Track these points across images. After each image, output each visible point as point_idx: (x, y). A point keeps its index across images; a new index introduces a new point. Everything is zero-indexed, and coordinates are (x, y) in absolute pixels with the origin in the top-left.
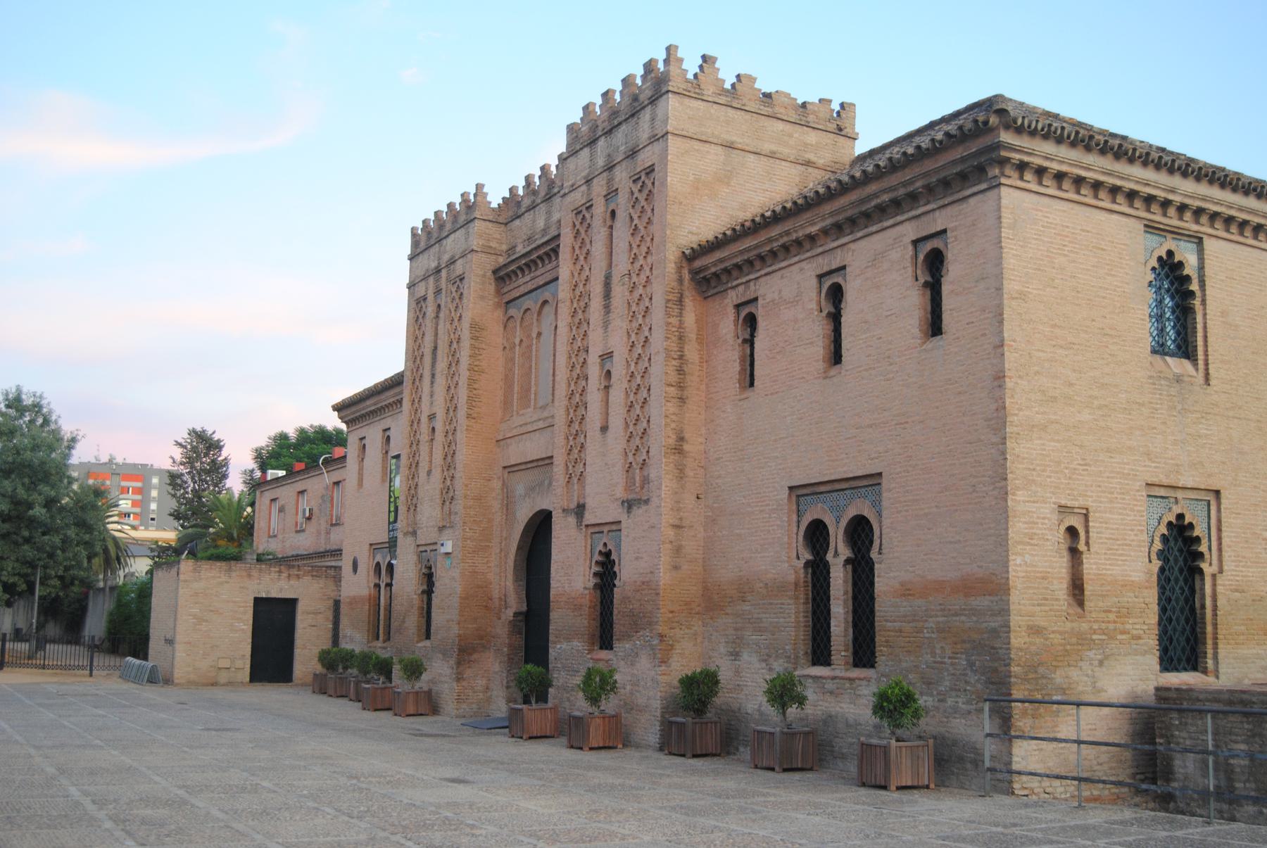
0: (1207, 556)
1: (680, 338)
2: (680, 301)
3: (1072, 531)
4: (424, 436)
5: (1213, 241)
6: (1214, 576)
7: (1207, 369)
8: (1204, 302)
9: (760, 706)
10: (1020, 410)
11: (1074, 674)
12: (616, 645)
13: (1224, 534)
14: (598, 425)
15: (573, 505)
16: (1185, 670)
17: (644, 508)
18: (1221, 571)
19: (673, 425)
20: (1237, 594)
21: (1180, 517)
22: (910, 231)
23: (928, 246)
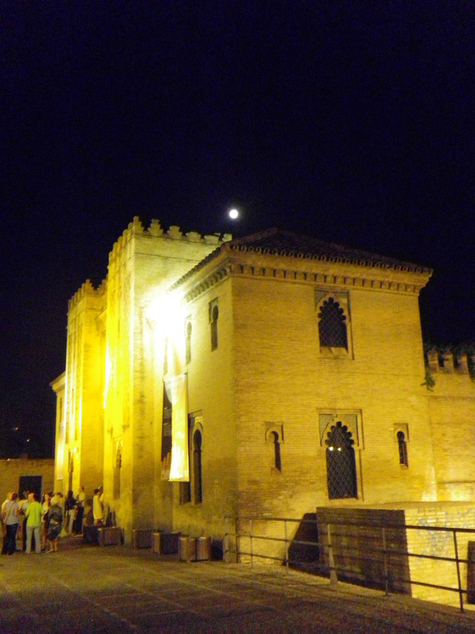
0: (356, 441)
1: (141, 350)
2: (141, 332)
3: (276, 434)
5: (355, 291)
6: (360, 451)
7: (353, 352)
8: (350, 320)
10: (242, 379)
11: (275, 502)
13: (364, 430)
16: (347, 497)
18: (364, 449)
19: (138, 390)
20: (374, 459)
21: (339, 424)
22: (95, 313)
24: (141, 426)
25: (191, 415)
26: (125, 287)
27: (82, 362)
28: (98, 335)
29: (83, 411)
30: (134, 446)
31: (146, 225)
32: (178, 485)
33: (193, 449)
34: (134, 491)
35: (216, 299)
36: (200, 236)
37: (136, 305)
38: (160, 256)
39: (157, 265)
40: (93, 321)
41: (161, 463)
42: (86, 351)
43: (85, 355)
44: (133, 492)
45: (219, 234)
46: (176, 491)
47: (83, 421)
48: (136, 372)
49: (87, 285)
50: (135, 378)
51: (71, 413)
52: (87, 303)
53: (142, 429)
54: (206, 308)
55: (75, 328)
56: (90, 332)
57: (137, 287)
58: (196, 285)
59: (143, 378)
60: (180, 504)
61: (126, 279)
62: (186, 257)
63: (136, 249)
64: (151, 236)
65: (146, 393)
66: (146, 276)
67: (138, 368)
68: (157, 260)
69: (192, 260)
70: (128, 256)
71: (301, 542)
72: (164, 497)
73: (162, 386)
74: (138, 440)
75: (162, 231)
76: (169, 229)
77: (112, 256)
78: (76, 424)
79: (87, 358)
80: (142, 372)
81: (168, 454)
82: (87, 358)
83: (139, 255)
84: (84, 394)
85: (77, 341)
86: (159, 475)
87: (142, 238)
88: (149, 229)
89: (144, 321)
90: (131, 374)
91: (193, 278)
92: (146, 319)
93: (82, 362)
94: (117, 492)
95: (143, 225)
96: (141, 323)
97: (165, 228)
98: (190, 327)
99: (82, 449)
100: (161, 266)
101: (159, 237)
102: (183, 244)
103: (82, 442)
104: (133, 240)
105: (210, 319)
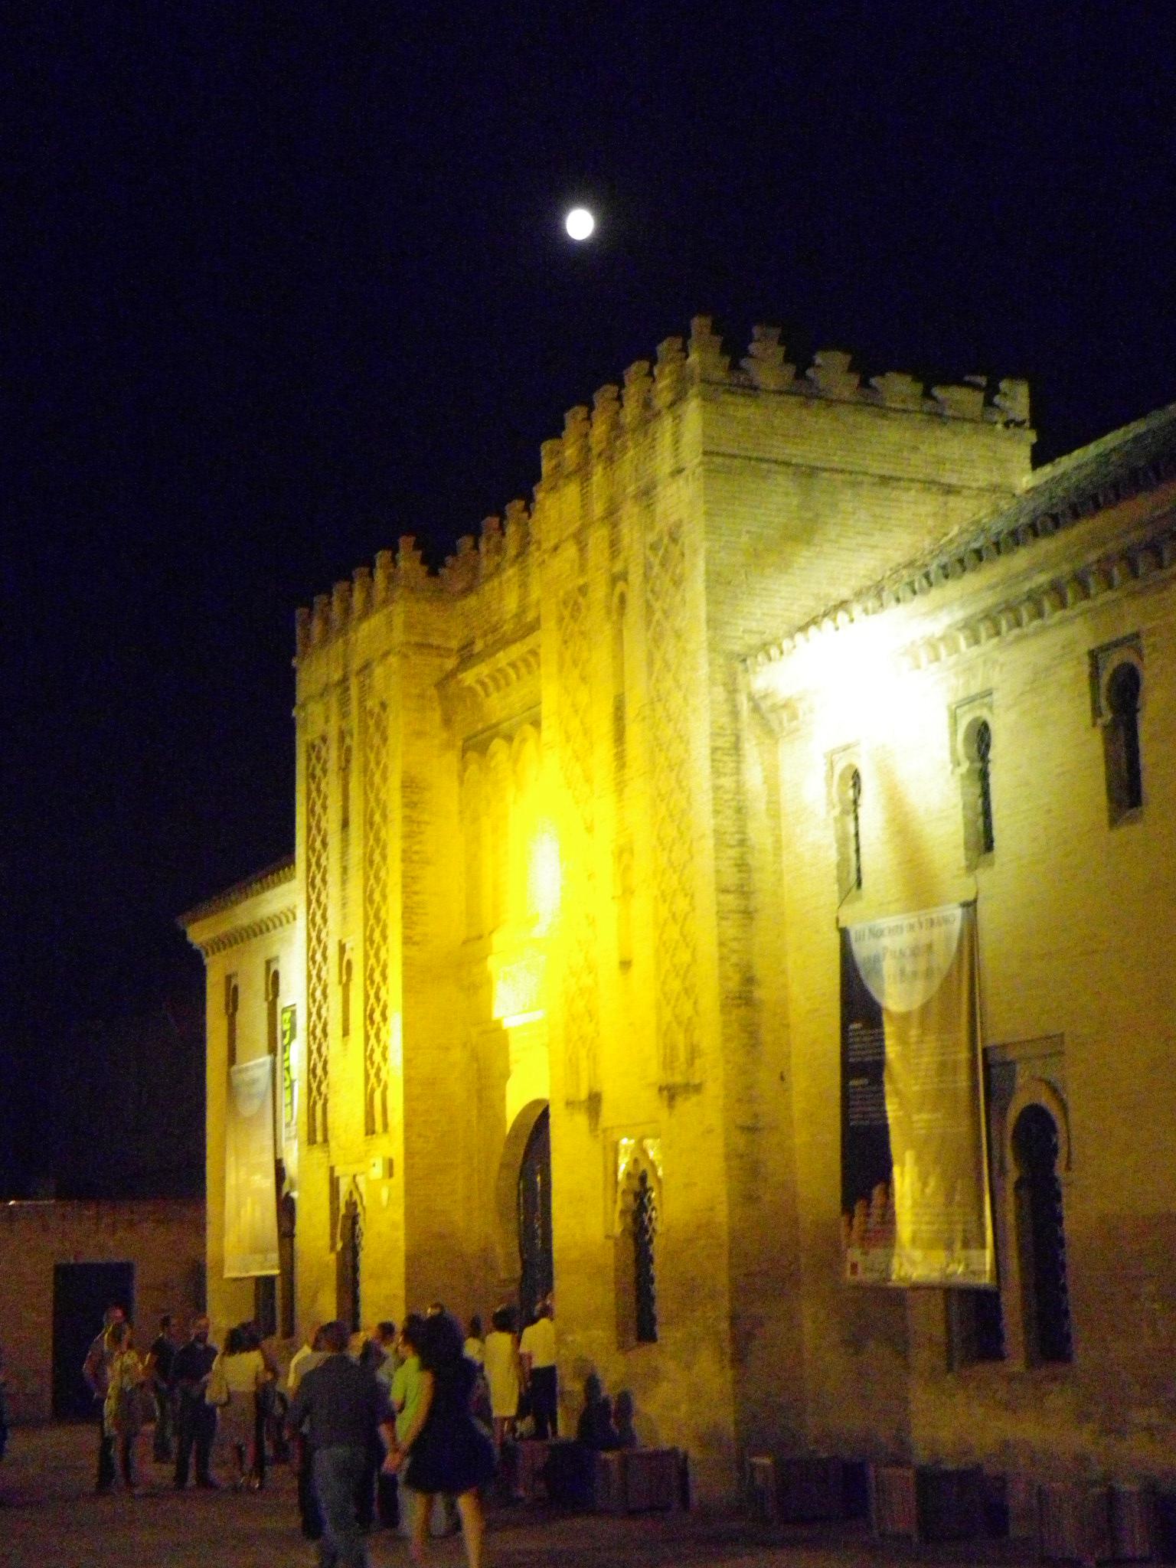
1: (739, 810)
2: (736, 747)
4: (331, 972)
9: (990, 708)
12: (661, 1332)
14: (636, 970)
15: (583, 1095)
17: (694, 1099)
19: (734, 959)
22: (437, 661)
23: (1115, 659)
24: (750, 1087)
25: (990, 1054)
26: (646, 577)
27: (395, 848)
28: (448, 746)
29: (407, 1026)
30: (727, 1157)
31: (735, 349)
32: (939, 1299)
33: (1013, 1174)
34: (734, 1319)
35: (1132, 640)
36: (918, 388)
37: (713, 648)
38: (787, 464)
39: (779, 498)
40: (432, 692)
41: (844, 1220)
42: (410, 805)
43: (408, 820)
44: (732, 1325)
45: (982, 380)
46: (929, 1324)
47: (408, 1062)
48: (724, 891)
49: (408, 560)
50: (722, 916)
51: (335, 1029)
52: (409, 627)
53: (751, 1100)
54: (1074, 673)
55: (345, 715)
56: (420, 734)
57: (716, 580)
58: (1027, 586)
59: (748, 915)
60: (950, 1368)
61: (654, 547)
62: (877, 468)
63: (707, 437)
64: (756, 389)
65: (759, 972)
66: (745, 538)
67: (731, 878)
68: (780, 479)
69: (899, 479)
70: (664, 464)
71: (376, 1485)
72: (855, 1343)
73: (835, 939)
74: (741, 1141)
75: (791, 369)
76: (810, 364)
77: (558, 455)
78: (372, 1075)
79: (413, 830)
80: (744, 891)
81: (877, 1192)
82: (413, 830)
83: (719, 460)
84: (407, 963)
85: (355, 766)
86: (832, 1258)
87: (728, 398)
88: (744, 363)
89: (745, 706)
90: (707, 899)
91: (1020, 559)
92: (751, 698)
93: (395, 848)
94: (640, 1322)
95: (725, 349)
96: (735, 714)
97: (799, 359)
98: (981, 738)
99: (409, 1167)
100: (795, 501)
101: (780, 393)
102: (863, 419)
103: (407, 1140)
104: (693, 411)
105: (1096, 712)
